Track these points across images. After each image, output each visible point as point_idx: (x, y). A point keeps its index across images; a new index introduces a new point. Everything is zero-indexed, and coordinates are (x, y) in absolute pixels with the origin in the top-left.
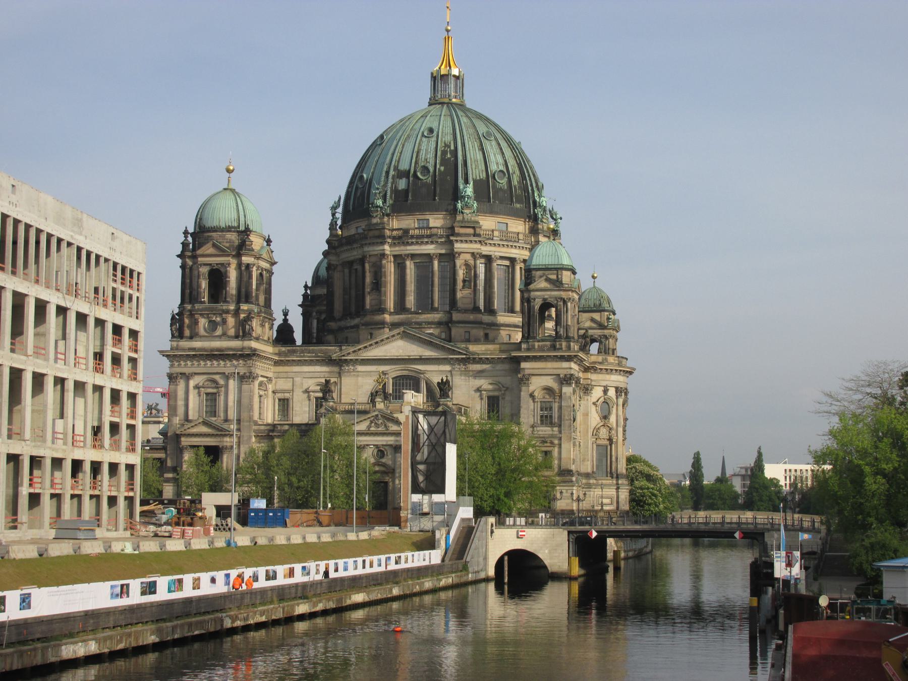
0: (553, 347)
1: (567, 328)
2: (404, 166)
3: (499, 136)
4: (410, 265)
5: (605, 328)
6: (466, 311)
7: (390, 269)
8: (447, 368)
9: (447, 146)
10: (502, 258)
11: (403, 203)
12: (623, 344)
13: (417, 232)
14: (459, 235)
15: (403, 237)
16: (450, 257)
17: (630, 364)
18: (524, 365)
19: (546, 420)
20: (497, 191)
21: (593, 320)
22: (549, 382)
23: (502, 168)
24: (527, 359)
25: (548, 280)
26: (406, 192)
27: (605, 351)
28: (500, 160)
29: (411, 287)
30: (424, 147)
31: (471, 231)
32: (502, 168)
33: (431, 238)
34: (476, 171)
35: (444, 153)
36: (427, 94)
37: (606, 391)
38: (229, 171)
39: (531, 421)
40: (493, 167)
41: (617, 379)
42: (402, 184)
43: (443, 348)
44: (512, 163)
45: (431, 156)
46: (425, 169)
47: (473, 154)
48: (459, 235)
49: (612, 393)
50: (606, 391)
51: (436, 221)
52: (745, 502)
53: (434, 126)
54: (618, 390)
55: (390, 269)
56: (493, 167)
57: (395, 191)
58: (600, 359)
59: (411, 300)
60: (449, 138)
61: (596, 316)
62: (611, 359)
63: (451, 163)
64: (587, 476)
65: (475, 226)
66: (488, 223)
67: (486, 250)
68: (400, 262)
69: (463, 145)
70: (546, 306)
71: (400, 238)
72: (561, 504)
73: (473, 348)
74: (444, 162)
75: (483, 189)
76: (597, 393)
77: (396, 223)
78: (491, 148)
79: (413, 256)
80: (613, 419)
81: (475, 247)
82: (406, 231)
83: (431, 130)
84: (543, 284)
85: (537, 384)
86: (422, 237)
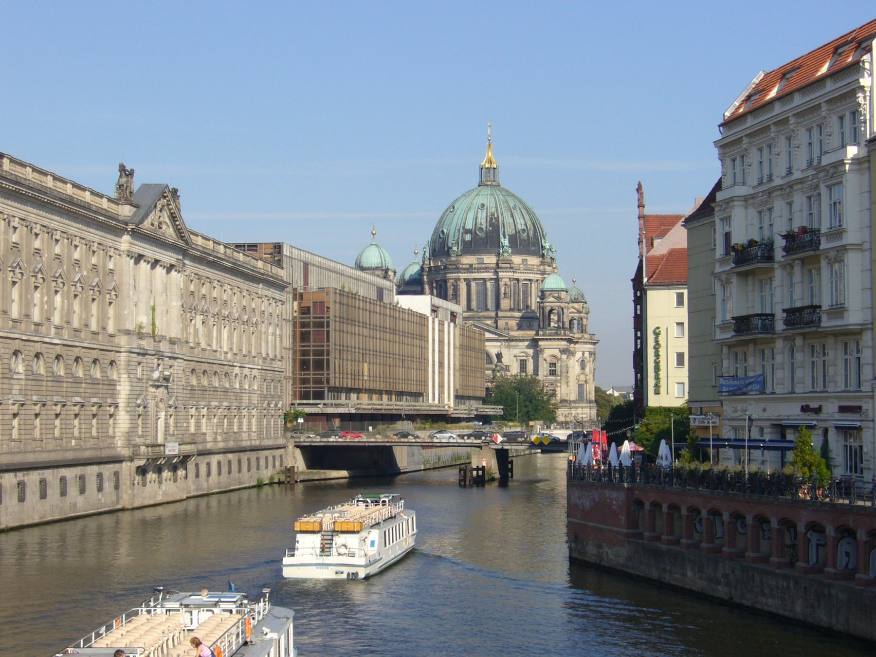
0: (556, 334)
1: (563, 323)
2: (469, 225)
3: (521, 206)
4: (473, 284)
5: (581, 313)
6: (506, 311)
7: (463, 286)
8: (499, 344)
9: (493, 214)
10: (525, 280)
11: (469, 248)
12: (591, 324)
13: (477, 266)
14: (501, 268)
15: (470, 269)
16: (497, 280)
17: (596, 338)
18: (540, 343)
19: (553, 373)
20: (521, 240)
21: (574, 308)
22: (556, 352)
23: (524, 227)
24: (543, 340)
25: (554, 297)
26: (470, 242)
27: (583, 330)
28: (523, 222)
29: (474, 297)
30: (479, 216)
31: (508, 265)
32: (524, 227)
33: (487, 269)
34: (510, 230)
35: (491, 219)
36: (477, 180)
37: (583, 354)
38: (373, 234)
39: (545, 373)
40: (519, 227)
41: (589, 347)
42: (468, 237)
43: (495, 334)
44: (529, 223)
45: (484, 221)
46: (481, 229)
47: (508, 220)
48: (501, 268)
49: (587, 354)
50: (583, 354)
51: (490, 260)
52: (855, 94)
53: (485, 202)
54: (591, 353)
55: (463, 286)
56: (519, 227)
57: (464, 241)
58: (580, 336)
59: (474, 304)
60: (493, 210)
61: (576, 305)
62: (586, 336)
63: (495, 225)
64: (574, 402)
65: (510, 262)
66: (517, 260)
67: (516, 276)
68: (468, 282)
69: (502, 214)
70: (551, 312)
71: (468, 269)
72: (561, 419)
73: (512, 333)
74: (491, 224)
75: (514, 240)
76: (579, 355)
77: (467, 260)
78: (517, 215)
79: (475, 279)
80: (587, 369)
81: (510, 274)
82: (471, 265)
83: (483, 205)
84: (552, 299)
85: (547, 353)
86: (480, 269)
